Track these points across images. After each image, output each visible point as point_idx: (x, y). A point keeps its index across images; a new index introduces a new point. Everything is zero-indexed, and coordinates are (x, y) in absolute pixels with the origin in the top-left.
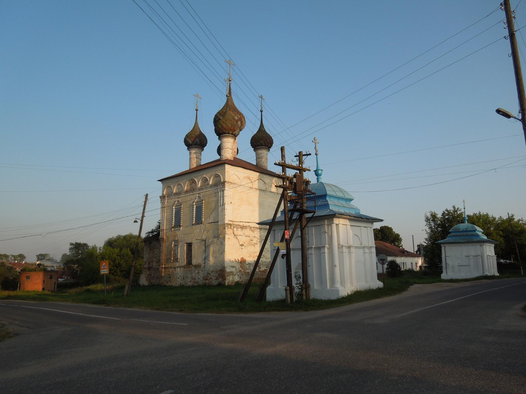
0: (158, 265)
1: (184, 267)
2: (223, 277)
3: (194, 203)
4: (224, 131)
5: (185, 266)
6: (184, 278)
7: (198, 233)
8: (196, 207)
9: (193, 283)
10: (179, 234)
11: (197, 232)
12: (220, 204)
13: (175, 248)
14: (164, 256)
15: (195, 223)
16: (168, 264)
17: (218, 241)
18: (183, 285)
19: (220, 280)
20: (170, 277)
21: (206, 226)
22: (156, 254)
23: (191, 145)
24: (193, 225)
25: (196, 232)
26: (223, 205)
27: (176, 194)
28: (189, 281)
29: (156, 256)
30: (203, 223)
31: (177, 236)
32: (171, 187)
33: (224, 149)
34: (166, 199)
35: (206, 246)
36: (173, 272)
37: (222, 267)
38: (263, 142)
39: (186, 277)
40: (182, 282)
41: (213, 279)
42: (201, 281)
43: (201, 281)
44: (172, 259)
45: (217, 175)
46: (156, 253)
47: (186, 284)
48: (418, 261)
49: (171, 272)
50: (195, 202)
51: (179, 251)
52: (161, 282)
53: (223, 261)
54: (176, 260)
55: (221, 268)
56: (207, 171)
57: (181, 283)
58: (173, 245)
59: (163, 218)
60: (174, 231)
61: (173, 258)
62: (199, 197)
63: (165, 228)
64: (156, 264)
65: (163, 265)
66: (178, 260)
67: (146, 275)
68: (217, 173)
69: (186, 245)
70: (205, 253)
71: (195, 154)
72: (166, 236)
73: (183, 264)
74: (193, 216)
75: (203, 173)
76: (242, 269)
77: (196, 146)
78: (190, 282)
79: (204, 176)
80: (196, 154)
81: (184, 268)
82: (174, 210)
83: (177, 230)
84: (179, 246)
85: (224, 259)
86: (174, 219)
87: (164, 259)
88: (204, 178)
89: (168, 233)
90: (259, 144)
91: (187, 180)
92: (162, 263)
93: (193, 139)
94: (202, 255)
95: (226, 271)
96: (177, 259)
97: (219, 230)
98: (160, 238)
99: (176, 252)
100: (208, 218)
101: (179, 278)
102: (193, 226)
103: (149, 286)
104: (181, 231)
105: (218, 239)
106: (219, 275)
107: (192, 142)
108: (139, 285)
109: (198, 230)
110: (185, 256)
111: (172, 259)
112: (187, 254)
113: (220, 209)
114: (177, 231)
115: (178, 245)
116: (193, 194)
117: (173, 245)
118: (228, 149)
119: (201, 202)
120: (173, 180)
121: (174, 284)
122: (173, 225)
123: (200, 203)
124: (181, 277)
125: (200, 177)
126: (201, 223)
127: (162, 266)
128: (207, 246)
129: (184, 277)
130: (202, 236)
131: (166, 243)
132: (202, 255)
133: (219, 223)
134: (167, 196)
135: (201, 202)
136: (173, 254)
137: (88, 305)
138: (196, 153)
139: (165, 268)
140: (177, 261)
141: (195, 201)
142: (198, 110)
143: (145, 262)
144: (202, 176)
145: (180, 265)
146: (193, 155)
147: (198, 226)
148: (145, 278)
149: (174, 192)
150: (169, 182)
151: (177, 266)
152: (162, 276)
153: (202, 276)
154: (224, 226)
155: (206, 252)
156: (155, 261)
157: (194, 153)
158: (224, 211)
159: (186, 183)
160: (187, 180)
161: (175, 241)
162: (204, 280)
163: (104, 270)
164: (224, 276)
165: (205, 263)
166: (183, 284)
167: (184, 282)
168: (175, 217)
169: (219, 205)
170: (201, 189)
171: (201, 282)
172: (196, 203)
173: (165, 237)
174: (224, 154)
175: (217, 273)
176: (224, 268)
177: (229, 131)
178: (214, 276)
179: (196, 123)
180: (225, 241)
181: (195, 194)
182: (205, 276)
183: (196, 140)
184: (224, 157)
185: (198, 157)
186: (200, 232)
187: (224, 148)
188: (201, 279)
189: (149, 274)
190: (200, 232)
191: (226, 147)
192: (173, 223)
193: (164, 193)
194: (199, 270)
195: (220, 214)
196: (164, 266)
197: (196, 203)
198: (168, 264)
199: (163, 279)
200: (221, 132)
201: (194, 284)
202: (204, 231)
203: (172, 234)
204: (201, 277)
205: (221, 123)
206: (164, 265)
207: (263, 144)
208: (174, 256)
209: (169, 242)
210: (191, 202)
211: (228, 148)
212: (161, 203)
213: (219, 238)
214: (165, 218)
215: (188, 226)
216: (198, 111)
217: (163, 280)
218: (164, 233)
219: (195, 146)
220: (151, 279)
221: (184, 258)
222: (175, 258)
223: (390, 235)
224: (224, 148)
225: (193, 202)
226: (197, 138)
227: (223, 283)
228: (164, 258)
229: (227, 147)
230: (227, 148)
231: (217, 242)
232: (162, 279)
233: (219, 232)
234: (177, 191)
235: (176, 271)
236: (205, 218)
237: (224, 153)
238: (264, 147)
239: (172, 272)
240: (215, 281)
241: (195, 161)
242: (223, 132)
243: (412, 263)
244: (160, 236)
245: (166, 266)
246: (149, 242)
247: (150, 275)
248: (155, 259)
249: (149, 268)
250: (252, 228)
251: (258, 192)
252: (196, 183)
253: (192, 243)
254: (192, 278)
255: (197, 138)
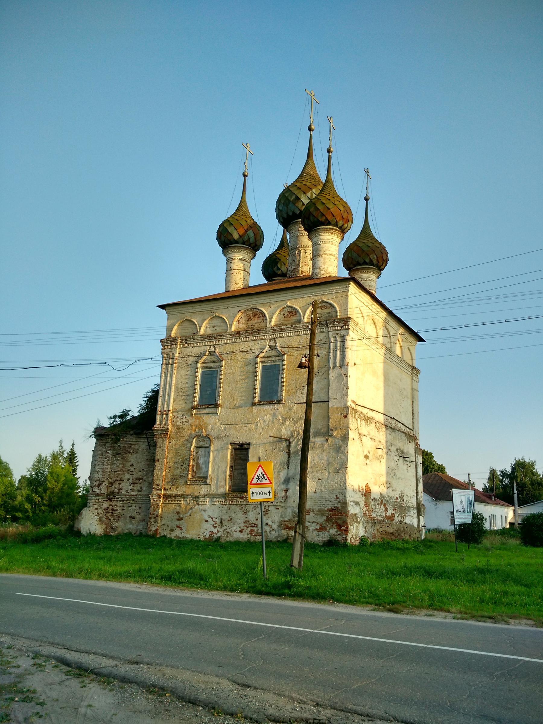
0: (135, 488)
1: (225, 498)
2: (339, 527)
3: (259, 360)
4: (330, 218)
5: (228, 494)
6: (221, 522)
7: (267, 423)
8: (263, 366)
9: (249, 536)
10: (212, 422)
11: (265, 421)
12: (335, 363)
13: (197, 453)
14: (164, 468)
15: (259, 401)
16: (176, 489)
17: (326, 445)
18: (218, 539)
19: (333, 531)
20: (180, 519)
21: (290, 409)
22: (132, 465)
23: (236, 242)
24: (254, 404)
25: (262, 422)
26: (341, 366)
27: (207, 337)
28: (239, 529)
29: (132, 469)
30: (283, 402)
31: (206, 428)
32: (192, 322)
33: (323, 256)
34: (178, 346)
35: (291, 453)
36: (189, 507)
37: (339, 502)
38: (375, 257)
39: (230, 520)
40: (215, 531)
41: (311, 528)
42: (273, 530)
43: (273, 530)
44: (190, 476)
45: (325, 304)
46: (131, 463)
47: (227, 537)
48: (507, 513)
49: (183, 506)
50: (261, 357)
51: (211, 460)
52: (154, 529)
53: (343, 488)
54: (204, 480)
55: (336, 505)
56: (297, 293)
57: (212, 533)
58: (192, 447)
59: (167, 387)
60: (198, 416)
61: (192, 474)
62: (273, 348)
63: (171, 408)
64: (130, 487)
65: (161, 490)
66: (208, 481)
67: (100, 511)
68: (324, 300)
69: (230, 447)
70: (286, 467)
71: (243, 263)
72: (172, 425)
73: (221, 491)
74: (255, 385)
75: (287, 298)
76: (367, 510)
77: (245, 246)
78: (241, 531)
79: (289, 303)
80: (245, 262)
81: (223, 500)
82: (200, 371)
83: (207, 413)
84: (212, 449)
85: (345, 483)
86: (198, 391)
87: (165, 475)
88: (288, 308)
89: (178, 419)
90: (367, 261)
91: (238, 309)
92: (158, 485)
93: (242, 231)
94: (279, 472)
95: (349, 512)
96: (206, 478)
97: (330, 421)
98: (157, 430)
99: (201, 461)
100: (298, 392)
101: (206, 521)
102: (254, 407)
103: (106, 536)
104: (217, 417)
105: (327, 440)
106: (329, 520)
107: (240, 236)
108: (78, 534)
109: (268, 418)
110: (228, 473)
111: (190, 476)
112: (231, 467)
113: (333, 374)
114: (206, 416)
115: (209, 447)
116: (256, 340)
117: (192, 447)
118: (331, 257)
119: (217, 364)
120: (198, 308)
121: (191, 534)
122: (195, 403)
123: (212, 365)
124: (212, 518)
125: (276, 305)
126: (279, 401)
127: (159, 492)
128: (293, 453)
129: (221, 519)
130: (279, 430)
131: (173, 442)
132: (279, 472)
133: (330, 405)
134: (182, 341)
135: (217, 364)
136: (193, 466)
137: (146, 588)
138: (244, 260)
139: (166, 497)
140: (206, 481)
141: (262, 355)
142: (247, 176)
143: (98, 482)
144: (283, 303)
145: (213, 490)
146: (236, 264)
147: (267, 407)
148: (97, 518)
149: (202, 332)
150: (187, 313)
151: (202, 493)
152: (157, 516)
153: (277, 519)
154: (345, 412)
155: (290, 465)
156: (128, 479)
157: (240, 259)
158: (345, 379)
159: (235, 316)
160: (238, 309)
161: (198, 436)
162: (285, 529)
163: (260, 490)
164: (345, 522)
165: (286, 491)
166: (219, 535)
167: (221, 530)
168: (200, 386)
169: (331, 365)
170: (279, 329)
171: (273, 533)
172: (263, 359)
173: (170, 427)
174: (323, 267)
175: (323, 515)
176: (345, 504)
177: (338, 220)
178: (313, 522)
179: (242, 203)
180: (347, 444)
181: (261, 339)
182: (286, 519)
183: (248, 233)
184: (322, 272)
185: (247, 268)
186: (273, 422)
187: (325, 254)
188: (275, 526)
189: (108, 508)
190: (273, 422)
191: (327, 252)
192: (197, 399)
193: (173, 334)
194: (269, 506)
195: (333, 385)
196: (162, 491)
197: (263, 359)
198: (175, 487)
199: (159, 522)
200: (320, 220)
201: (253, 538)
202: (284, 420)
203: (190, 421)
204: (274, 522)
205: (324, 202)
206: (165, 489)
207: (375, 262)
208: (195, 470)
209: (182, 440)
210: (251, 356)
211: (331, 255)
212: (162, 353)
213: (331, 436)
214: (173, 388)
215: (240, 407)
216: (247, 178)
217: (159, 525)
218: (169, 418)
219: (243, 245)
220: (112, 519)
221: (226, 476)
222: (198, 475)
223: (431, 466)
224: (325, 254)
225: (257, 357)
226: (251, 230)
227: (340, 538)
228: (164, 474)
229: (330, 252)
230: (329, 254)
231: (323, 445)
232: (156, 522)
233: (330, 424)
234: (210, 331)
235: (198, 504)
236: (288, 392)
237: (324, 263)
238: (367, 266)
239: (186, 508)
240: (316, 532)
241: (242, 276)
242: (327, 219)
243: (501, 516)
244: (155, 424)
245: (169, 492)
246: (113, 437)
247: (110, 510)
248: (127, 476)
249: (110, 496)
250: (378, 423)
251: (383, 351)
252: (197, 327)
253: (249, 444)
254: (245, 522)
255: (251, 230)
